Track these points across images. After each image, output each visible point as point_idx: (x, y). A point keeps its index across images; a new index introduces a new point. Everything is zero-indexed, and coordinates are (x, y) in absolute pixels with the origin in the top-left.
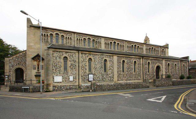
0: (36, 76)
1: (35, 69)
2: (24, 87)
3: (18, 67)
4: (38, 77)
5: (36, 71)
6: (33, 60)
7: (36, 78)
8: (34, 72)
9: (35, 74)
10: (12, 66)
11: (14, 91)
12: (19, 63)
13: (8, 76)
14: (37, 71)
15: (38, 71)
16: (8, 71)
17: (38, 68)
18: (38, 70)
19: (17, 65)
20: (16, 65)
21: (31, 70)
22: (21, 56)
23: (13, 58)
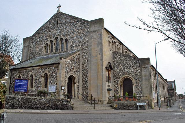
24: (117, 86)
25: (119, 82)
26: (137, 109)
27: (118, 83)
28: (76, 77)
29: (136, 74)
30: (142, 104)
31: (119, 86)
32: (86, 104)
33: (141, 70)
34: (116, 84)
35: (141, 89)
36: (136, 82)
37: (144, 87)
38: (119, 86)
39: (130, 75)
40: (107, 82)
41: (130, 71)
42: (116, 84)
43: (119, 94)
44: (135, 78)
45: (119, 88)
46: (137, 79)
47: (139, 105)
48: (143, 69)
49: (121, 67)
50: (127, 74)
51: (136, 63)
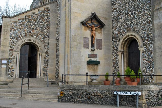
0: (89, 63)
1: (86, 47)
2: (121, 93)
3: (27, 39)
4: (93, 66)
5: (88, 51)
6: (83, 27)
7: (89, 69)
8: (85, 54)
9: (88, 59)
10: (17, 38)
11: (77, 102)
12: (30, 32)
13: (8, 60)
14: (90, 53)
15: (92, 53)
16: (8, 49)
17: (93, 45)
18: (92, 50)
19: (26, 34)
20: (24, 35)
21: (80, 48)
22: (36, 16)
23: (19, 20)
24: (117, 56)
25: (120, 48)
26: (114, 103)
27: (117, 51)
28: (40, 44)
29: (144, 28)
30: (133, 93)
31: (120, 54)
32: (48, 87)
33: (152, 16)
34: (115, 51)
35: (153, 59)
36: (144, 45)
37: (157, 54)
38: (120, 54)
39: (134, 31)
40: (88, 48)
41: (134, 22)
42: (115, 51)
43: (120, 70)
44: (141, 37)
45: (120, 59)
46: (145, 39)
47: (119, 95)
48: (155, 13)
49: (121, 18)
50: (129, 30)
51: (144, 5)
